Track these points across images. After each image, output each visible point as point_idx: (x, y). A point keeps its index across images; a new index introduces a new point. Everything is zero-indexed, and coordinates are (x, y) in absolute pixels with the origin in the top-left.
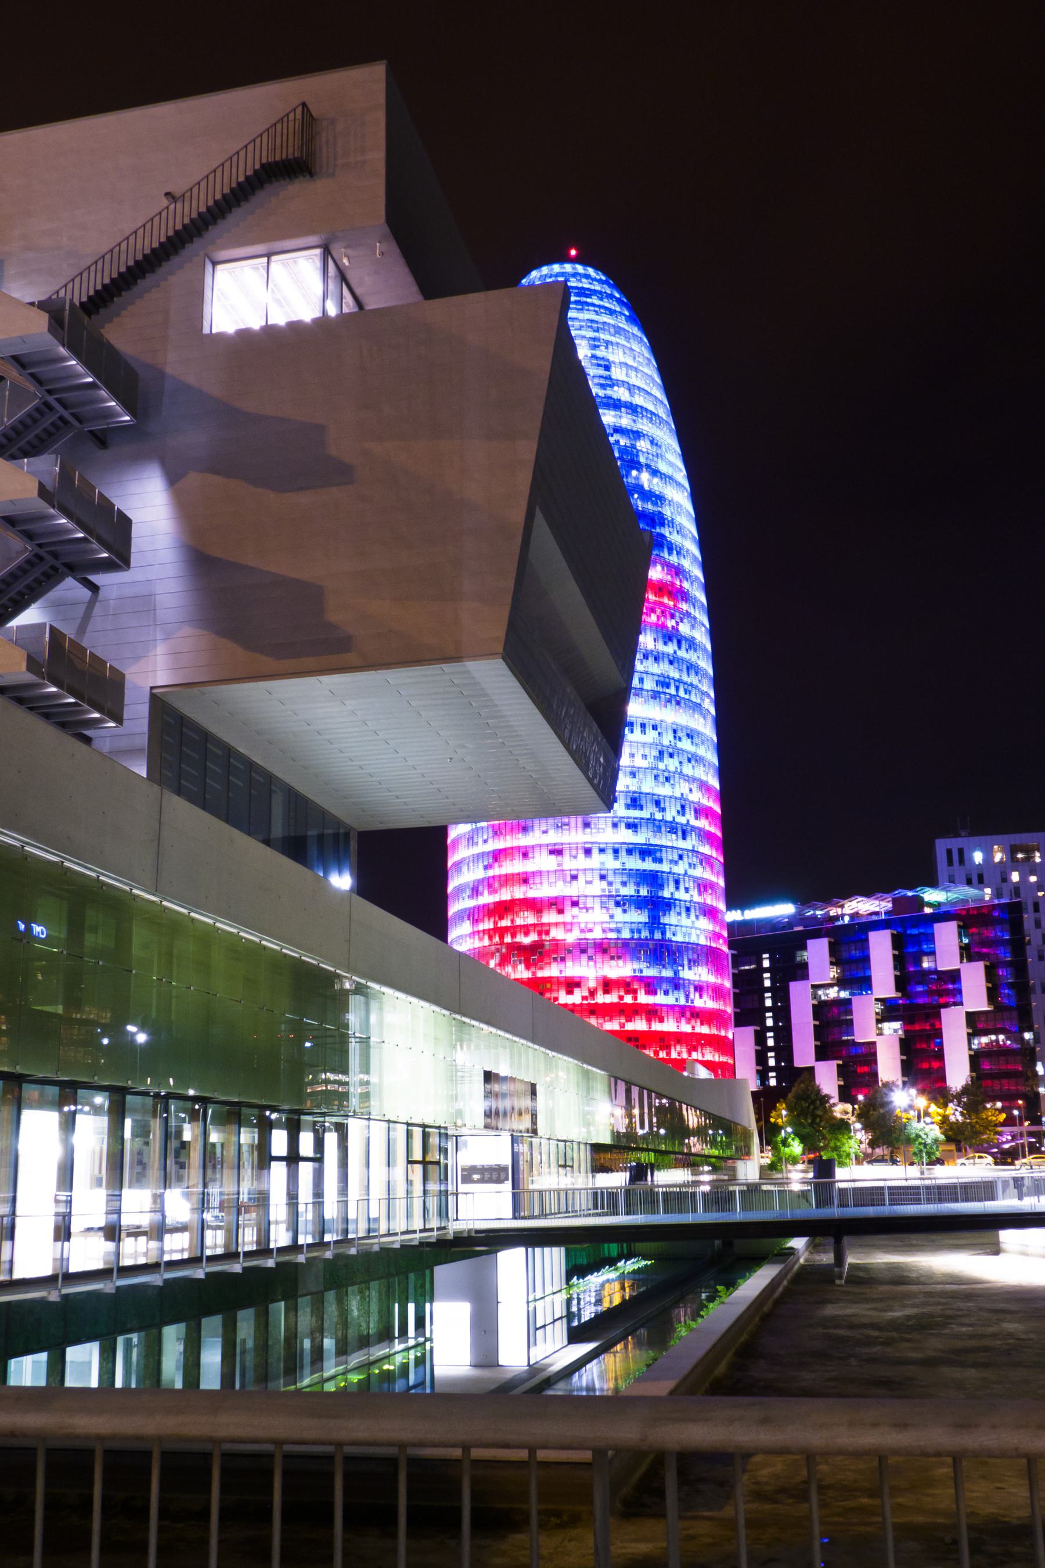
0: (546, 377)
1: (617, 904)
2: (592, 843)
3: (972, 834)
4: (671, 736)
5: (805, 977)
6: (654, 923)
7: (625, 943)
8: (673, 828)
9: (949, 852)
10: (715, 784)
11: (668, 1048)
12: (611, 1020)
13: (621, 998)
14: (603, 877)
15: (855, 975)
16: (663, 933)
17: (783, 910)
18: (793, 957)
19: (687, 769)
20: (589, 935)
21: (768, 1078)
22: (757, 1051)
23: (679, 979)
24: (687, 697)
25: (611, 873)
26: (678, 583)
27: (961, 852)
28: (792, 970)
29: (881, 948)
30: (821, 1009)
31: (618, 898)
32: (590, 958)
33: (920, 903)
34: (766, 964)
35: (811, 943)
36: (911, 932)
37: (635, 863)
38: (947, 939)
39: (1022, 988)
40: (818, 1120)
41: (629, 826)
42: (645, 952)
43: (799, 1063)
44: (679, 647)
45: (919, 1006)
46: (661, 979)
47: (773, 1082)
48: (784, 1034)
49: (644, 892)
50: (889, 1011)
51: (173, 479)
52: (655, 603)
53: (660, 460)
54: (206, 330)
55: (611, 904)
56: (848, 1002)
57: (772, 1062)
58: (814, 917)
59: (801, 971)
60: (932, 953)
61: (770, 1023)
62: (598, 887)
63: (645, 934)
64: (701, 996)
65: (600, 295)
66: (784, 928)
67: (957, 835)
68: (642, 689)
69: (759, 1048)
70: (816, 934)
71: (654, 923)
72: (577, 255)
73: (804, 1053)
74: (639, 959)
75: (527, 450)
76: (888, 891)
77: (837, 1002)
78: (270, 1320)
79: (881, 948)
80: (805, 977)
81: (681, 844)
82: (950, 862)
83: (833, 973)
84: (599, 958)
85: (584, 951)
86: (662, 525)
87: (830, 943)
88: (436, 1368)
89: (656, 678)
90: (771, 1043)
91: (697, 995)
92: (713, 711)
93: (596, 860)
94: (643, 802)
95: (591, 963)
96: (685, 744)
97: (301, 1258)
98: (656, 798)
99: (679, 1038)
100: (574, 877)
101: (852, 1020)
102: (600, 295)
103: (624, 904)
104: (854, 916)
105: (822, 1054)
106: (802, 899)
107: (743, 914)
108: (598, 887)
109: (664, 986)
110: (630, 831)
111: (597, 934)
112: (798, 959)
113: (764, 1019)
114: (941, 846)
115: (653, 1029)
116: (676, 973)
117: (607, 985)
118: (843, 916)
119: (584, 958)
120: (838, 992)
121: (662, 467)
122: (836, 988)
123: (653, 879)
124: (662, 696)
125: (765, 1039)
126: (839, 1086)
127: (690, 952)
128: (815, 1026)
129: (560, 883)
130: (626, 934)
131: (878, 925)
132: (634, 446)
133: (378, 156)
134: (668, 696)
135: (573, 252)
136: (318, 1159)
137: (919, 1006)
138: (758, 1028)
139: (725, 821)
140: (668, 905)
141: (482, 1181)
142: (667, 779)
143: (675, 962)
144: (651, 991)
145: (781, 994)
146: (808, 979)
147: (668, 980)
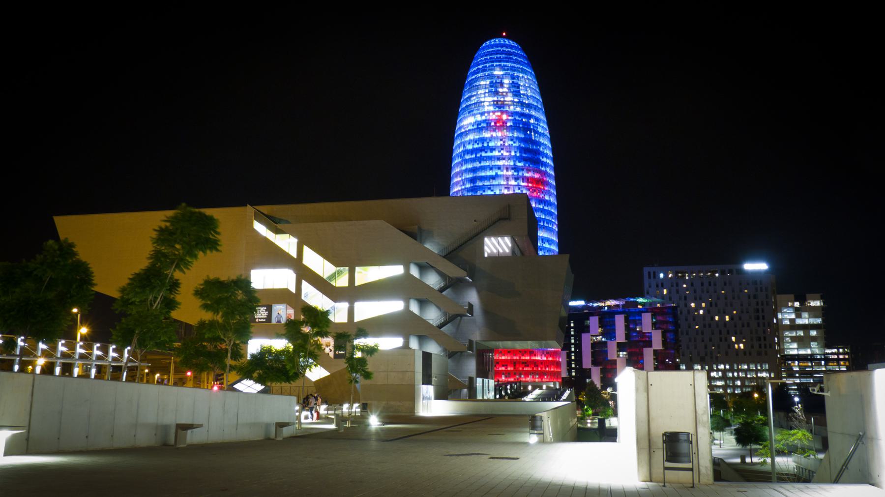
3: (660, 266)
5: (588, 332)
9: (649, 273)
11: (537, 367)
15: (609, 332)
17: (581, 303)
18: (583, 322)
27: (654, 273)
28: (582, 328)
29: (620, 321)
34: (572, 325)
35: (591, 318)
36: (632, 316)
38: (647, 319)
39: (677, 340)
43: (584, 367)
47: (574, 374)
48: (579, 355)
50: (621, 347)
51: (479, 292)
56: (605, 343)
57: (573, 366)
59: (587, 329)
61: (573, 349)
65: (516, 55)
67: (653, 266)
70: (592, 314)
73: (587, 363)
76: (624, 298)
77: (601, 342)
78: (788, 486)
79: (620, 321)
80: (588, 332)
82: (650, 277)
83: (600, 330)
88: (701, 478)
90: (573, 358)
99: (542, 362)
102: (516, 55)
104: (609, 307)
105: (595, 363)
106: (588, 300)
114: (646, 270)
121: (540, 130)
145: (578, 337)
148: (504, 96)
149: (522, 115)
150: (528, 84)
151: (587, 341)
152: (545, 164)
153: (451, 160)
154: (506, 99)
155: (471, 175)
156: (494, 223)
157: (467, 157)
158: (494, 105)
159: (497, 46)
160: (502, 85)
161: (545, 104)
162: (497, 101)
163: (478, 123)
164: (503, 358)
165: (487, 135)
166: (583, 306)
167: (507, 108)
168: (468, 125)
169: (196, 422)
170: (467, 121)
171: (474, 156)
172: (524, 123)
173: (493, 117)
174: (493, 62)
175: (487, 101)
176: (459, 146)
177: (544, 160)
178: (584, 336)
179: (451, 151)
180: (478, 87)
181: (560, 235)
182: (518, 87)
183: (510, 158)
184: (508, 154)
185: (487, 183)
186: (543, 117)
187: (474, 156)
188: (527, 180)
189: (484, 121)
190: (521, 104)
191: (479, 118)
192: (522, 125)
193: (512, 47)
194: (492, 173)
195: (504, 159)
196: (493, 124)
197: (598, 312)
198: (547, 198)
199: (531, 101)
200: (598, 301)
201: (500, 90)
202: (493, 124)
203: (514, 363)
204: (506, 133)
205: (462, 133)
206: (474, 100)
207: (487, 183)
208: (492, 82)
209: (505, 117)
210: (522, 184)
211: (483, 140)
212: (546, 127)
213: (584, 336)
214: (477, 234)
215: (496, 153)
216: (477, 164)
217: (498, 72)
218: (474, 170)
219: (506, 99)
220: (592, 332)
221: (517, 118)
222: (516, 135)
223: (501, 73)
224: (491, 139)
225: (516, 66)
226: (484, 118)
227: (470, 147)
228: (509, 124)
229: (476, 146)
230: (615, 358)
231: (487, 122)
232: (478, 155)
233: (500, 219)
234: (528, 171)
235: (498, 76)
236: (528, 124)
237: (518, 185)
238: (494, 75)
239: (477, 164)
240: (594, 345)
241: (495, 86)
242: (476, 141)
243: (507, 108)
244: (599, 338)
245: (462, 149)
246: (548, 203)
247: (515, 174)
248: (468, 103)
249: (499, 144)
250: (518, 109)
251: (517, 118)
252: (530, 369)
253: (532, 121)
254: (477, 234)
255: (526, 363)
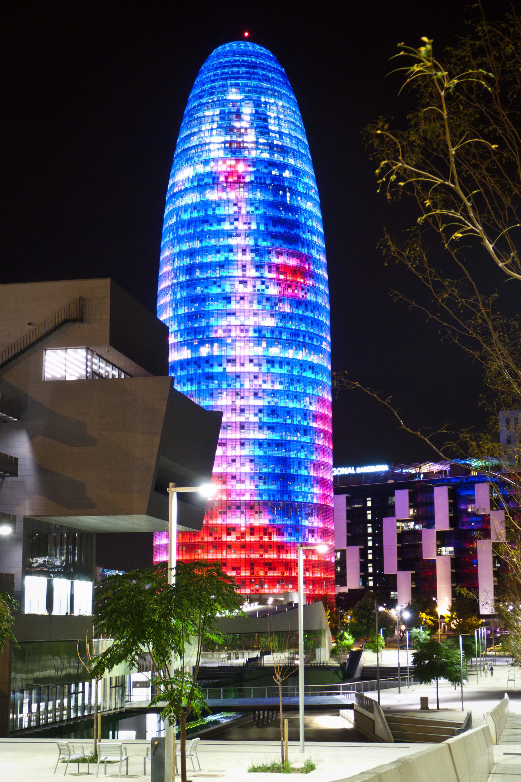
0: (164, 413)
1: (260, 478)
2: (245, 439)
4: (298, 369)
5: (393, 514)
6: (284, 491)
7: (265, 504)
8: (298, 429)
10: (329, 397)
12: (254, 552)
13: (261, 538)
14: (251, 461)
15: (426, 517)
16: (290, 497)
18: (387, 501)
19: (309, 391)
20: (243, 498)
21: (368, 581)
22: (361, 563)
23: (299, 525)
24: (310, 342)
25: (256, 459)
26: (307, 267)
29: (441, 497)
30: (402, 536)
31: (261, 475)
32: (243, 512)
33: (467, 470)
34: (369, 504)
35: (397, 492)
36: (461, 489)
37: (273, 453)
40: (371, 621)
41: (269, 428)
42: (278, 509)
44: (306, 309)
45: (463, 534)
46: (287, 526)
47: (371, 584)
48: (379, 551)
49: (278, 471)
50: (443, 539)
51: (31, 438)
52: (291, 281)
53: (298, 183)
54: (43, 380)
55: (256, 478)
57: (371, 570)
58: (401, 474)
60: (473, 502)
61: (370, 544)
62: (247, 468)
63: (278, 497)
64: (313, 536)
66: (381, 480)
68: (280, 339)
69: (363, 560)
71: (284, 491)
72: (248, 36)
73: (391, 565)
74: (274, 513)
75: (157, 440)
79: (441, 497)
81: (304, 439)
84: (247, 512)
85: (238, 508)
86: (298, 227)
87: (410, 493)
89: (290, 331)
90: (370, 557)
91: (310, 535)
92: (329, 349)
93: (247, 451)
94: (279, 412)
95: (243, 515)
96: (309, 374)
97: (79, 721)
98: (287, 409)
100: (234, 461)
101: (421, 544)
103: (265, 478)
104: (426, 474)
105: (402, 566)
106: (394, 461)
107: (355, 470)
108: (247, 468)
109: (289, 530)
110: (270, 431)
111: (247, 497)
112: (390, 502)
113: (367, 541)
115: (281, 557)
116: (297, 521)
117: (252, 530)
118: (419, 474)
119: (239, 512)
120: (414, 525)
122: (413, 523)
123: (285, 462)
124: (294, 343)
125: (367, 554)
126: (412, 588)
127: (307, 509)
128: (398, 547)
129: (225, 465)
130: (265, 498)
131: (440, 483)
132: (281, 175)
133: (107, 317)
134: (297, 343)
135: (246, 34)
136: (83, 692)
137: (463, 534)
138: (362, 547)
139: (335, 422)
140: (294, 478)
141: (140, 687)
142: (295, 397)
143: (296, 514)
144: (280, 533)
145: (377, 525)
146: (395, 516)
147: (292, 526)
148: (241, 135)
149: (271, 164)
150: (284, 115)
151: (392, 527)
152: (309, 245)
153: (158, 236)
154: (246, 138)
155: (186, 262)
156: (57, 327)
157: (182, 232)
158: (225, 148)
159: (234, 53)
160: (238, 115)
161: (313, 147)
162: (231, 143)
163: (199, 178)
164: (234, 556)
165: (212, 196)
166: (386, 472)
167: (246, 154)
168: (183, 182)
169: (494, 672)
170: (183, 175)
171: (192, 231)
172: (274, 178)
173: (222, 167)
174: (225, 79)
175: (215, 142)
176: (171, 216)
177: (308, 236)
178: (386, 521)
179: (161, 221)
180: (201, 120)
181: (334, 358)
182: (265, 120)
183: (249, 234)
184: (246, 227)
185: (210, 274)
186: (308, 168)
187: (192, 231)
188: (278, 269)
189: (209, 174)
190: (271, 147)
191: (201, 169)
192: (270, 181)
193: (257, 55)
194: (220, 258)
195: (239, 235)
196: (222, 179)
197: (407, 483)
198: (310, 297)
199: (287, 142)
200: (410, 465)
201: (237, 125)
202: (222, 179)
203: (251, 564)
204: (242, 193)
205: (175, 194)
206: (195, 141)
207: (210, 274)
208: (222, 113)
209: (241, 168)
210: (267, 275)
211: (205, 204)
212: (312, 183)
213: (386, 521)
214: (31, 345)
215: (226, 226)
216: (197, 244)
217: (233, 95)
218: (191, 253)
219: (246, 138)
220: (399, 516)
221: (263, 169)
222: (259, 195)
223: (240, 97)
224: (219, 203)
225: (265, 85)
226: (208, 169)
227: (186, 216)
228: (248, 179)
229: (195, 215)
230: (434, 557)
231: (214, 177)
232: (199, 230)
233: (66, 321)
234: (279, 254)
235: (234, 102)
236: (279, 179)
237: (261, 277)
238: (228, 101)
239: (197, 244)
240: (402, 536)
241: (227, 121)
242: (195, 207)
243: (246, 154)
244: (411, 525)
245: (174, 220)
246: (316, 307)
247: (257, 259)
248: (187, 146)
249: (231, 212)
250: (266, 155)
251: (263, 169)
252: (276, 574)
253: (287, 174)
254: (31, 345)
255: (271, 565)
